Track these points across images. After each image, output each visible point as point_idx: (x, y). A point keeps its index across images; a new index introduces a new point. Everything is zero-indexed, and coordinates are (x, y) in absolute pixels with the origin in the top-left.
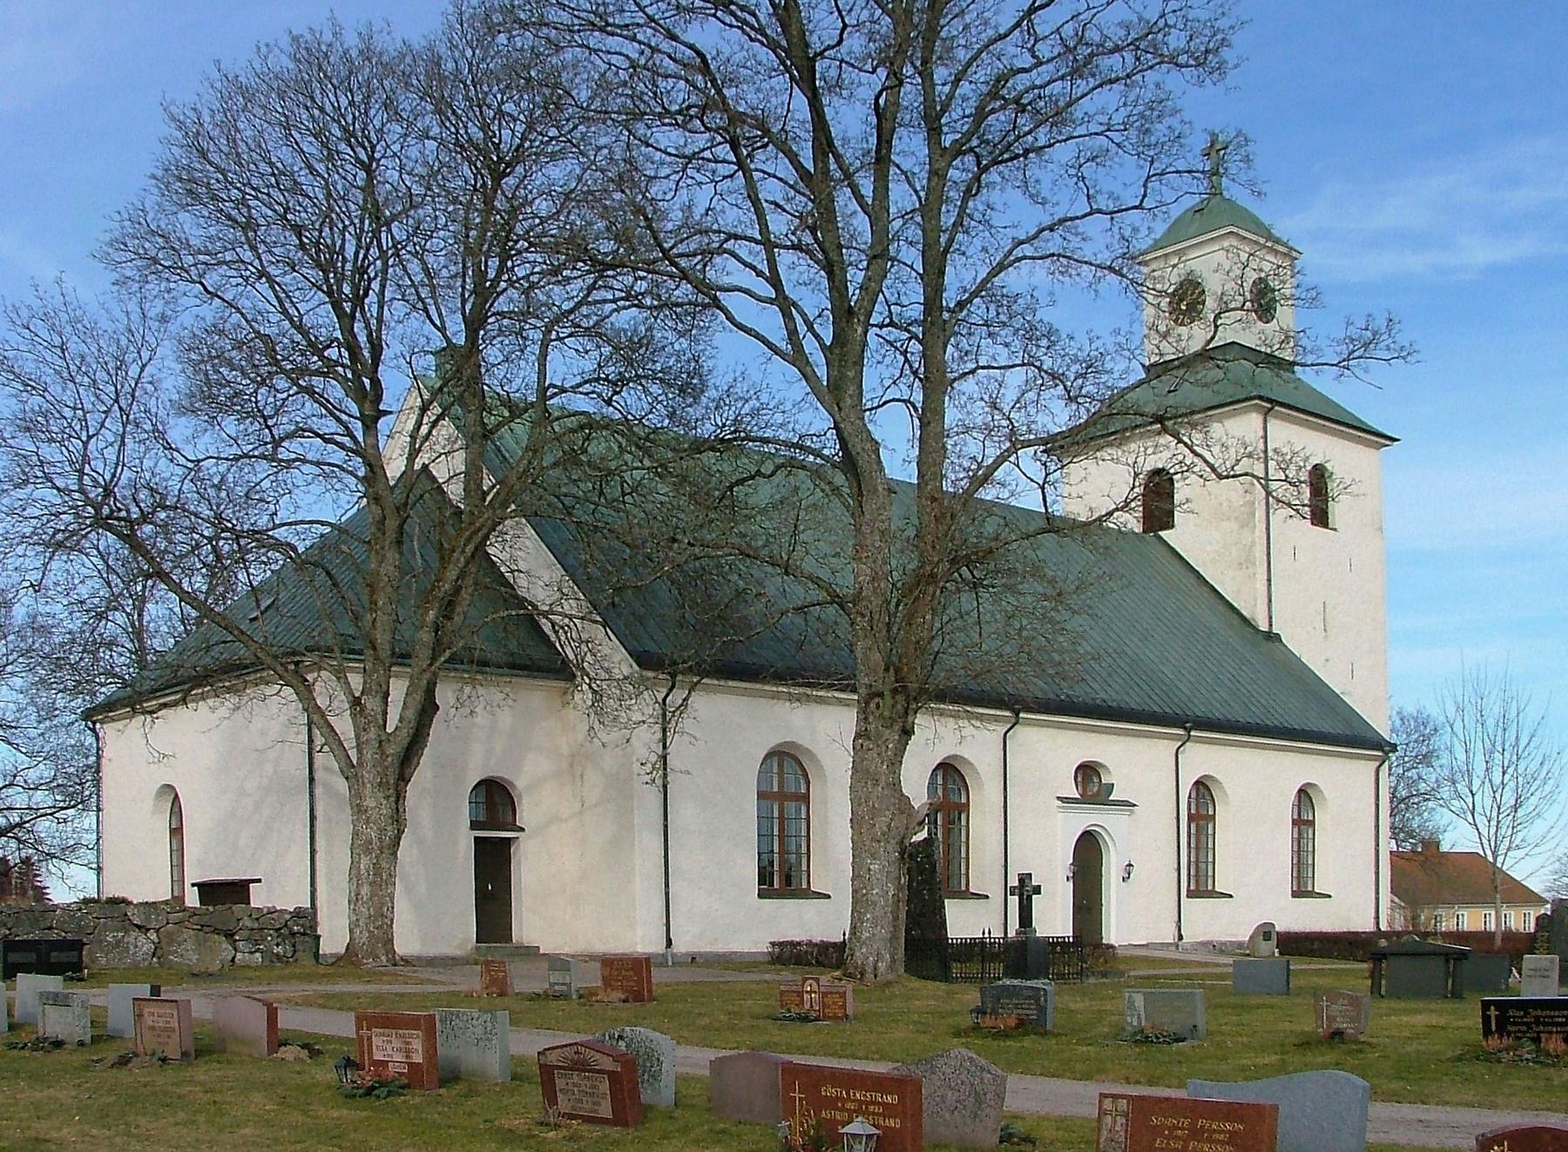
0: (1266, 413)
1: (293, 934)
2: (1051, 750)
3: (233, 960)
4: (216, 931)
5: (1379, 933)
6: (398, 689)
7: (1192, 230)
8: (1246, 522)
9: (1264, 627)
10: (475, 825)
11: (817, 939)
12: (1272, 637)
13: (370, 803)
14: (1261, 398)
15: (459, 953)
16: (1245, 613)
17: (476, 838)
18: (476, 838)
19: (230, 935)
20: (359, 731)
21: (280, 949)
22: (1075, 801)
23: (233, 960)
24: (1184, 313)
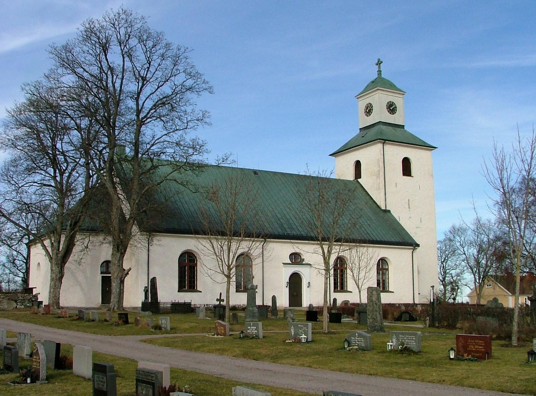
0: (384, 143)
1: (33, 301)
2: (281, 250)
3: (16, 307)
4: (12, 300)
5: (414, 305)
6: (63, 239)
7: (370, 88)
8: (378, 176)
9: (383, 208)
10: (102, 273)
11: (392, 303)
12: (387, 212)
13: (54, 269)
14: (379, 139)
15: (96, 307)
16: (378, 204)
17: (102, 277)
18: (102, 277)
19: (16, 301)
20: (52, 251)
21: (28, 305)
22: (289, 264)
23: (16, 307)
24: (367, 113)
